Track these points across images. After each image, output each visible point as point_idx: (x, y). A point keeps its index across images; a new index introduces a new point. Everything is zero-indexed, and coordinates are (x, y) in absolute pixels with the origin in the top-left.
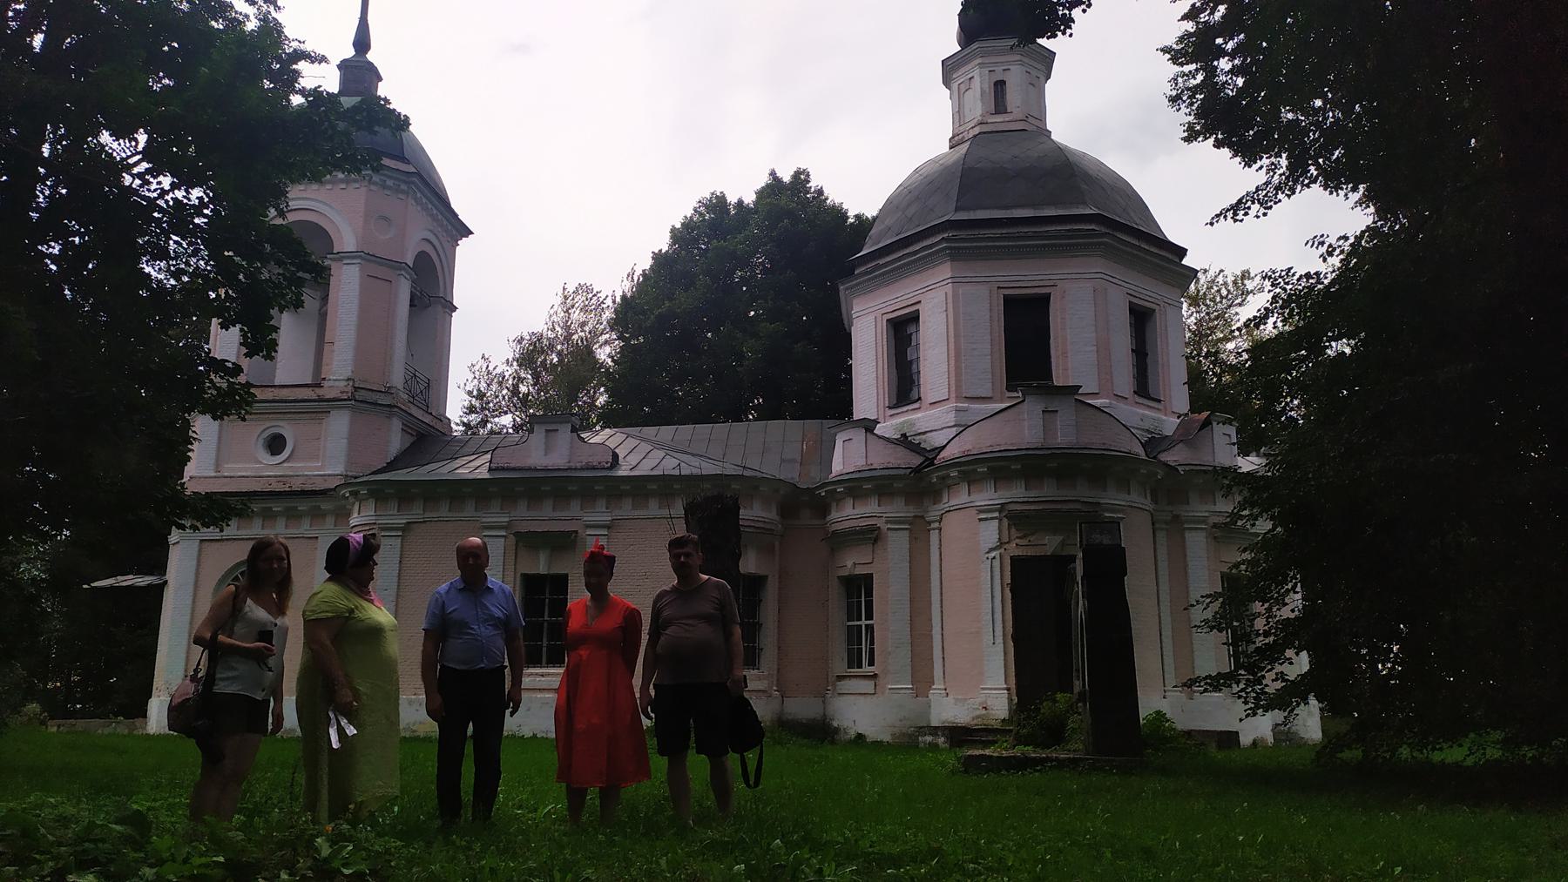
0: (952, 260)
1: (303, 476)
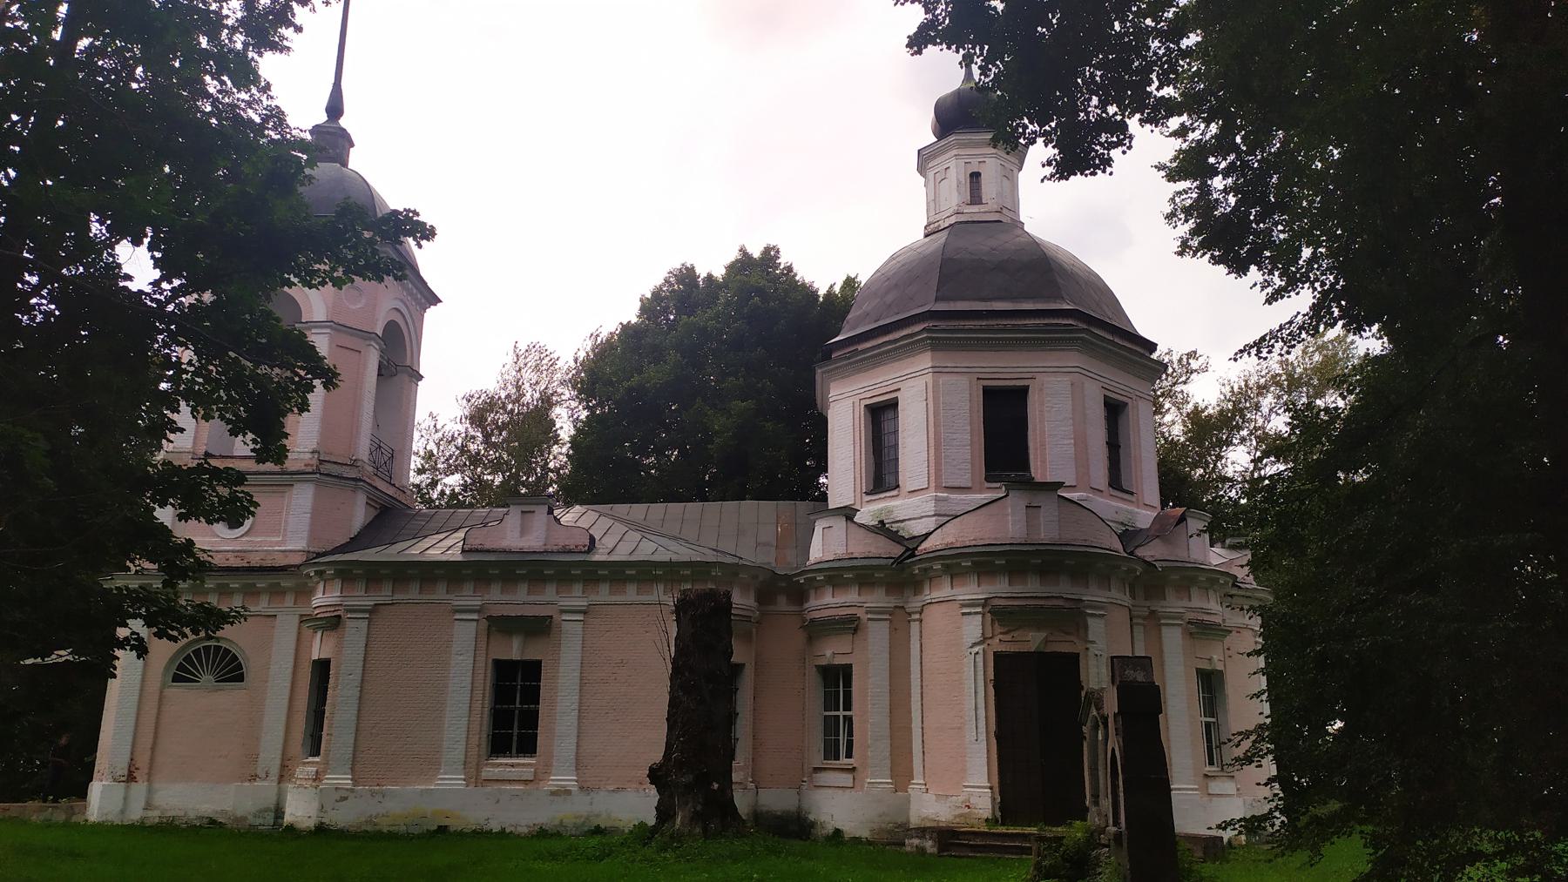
0: (932, 350)
1: (263, 551)
